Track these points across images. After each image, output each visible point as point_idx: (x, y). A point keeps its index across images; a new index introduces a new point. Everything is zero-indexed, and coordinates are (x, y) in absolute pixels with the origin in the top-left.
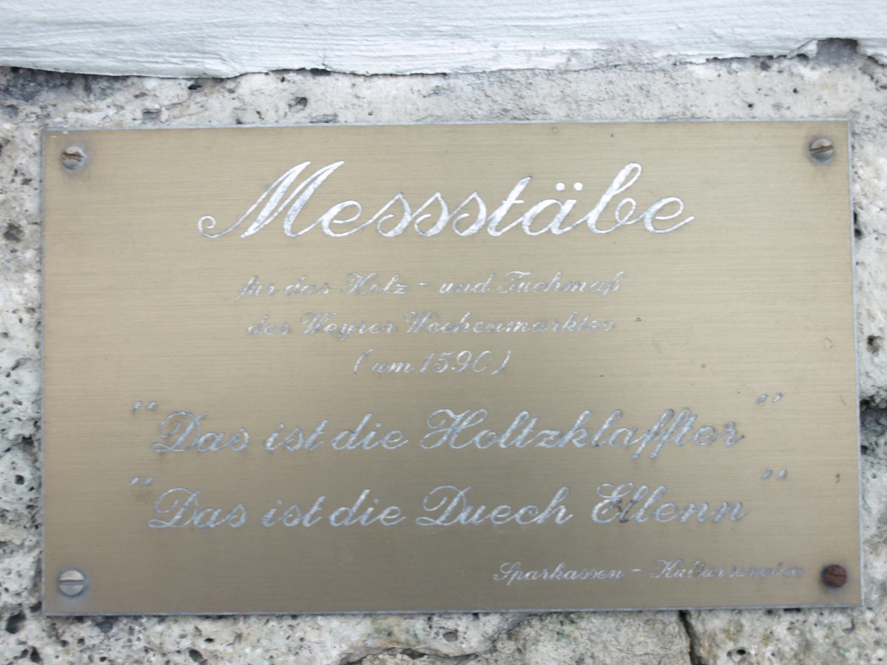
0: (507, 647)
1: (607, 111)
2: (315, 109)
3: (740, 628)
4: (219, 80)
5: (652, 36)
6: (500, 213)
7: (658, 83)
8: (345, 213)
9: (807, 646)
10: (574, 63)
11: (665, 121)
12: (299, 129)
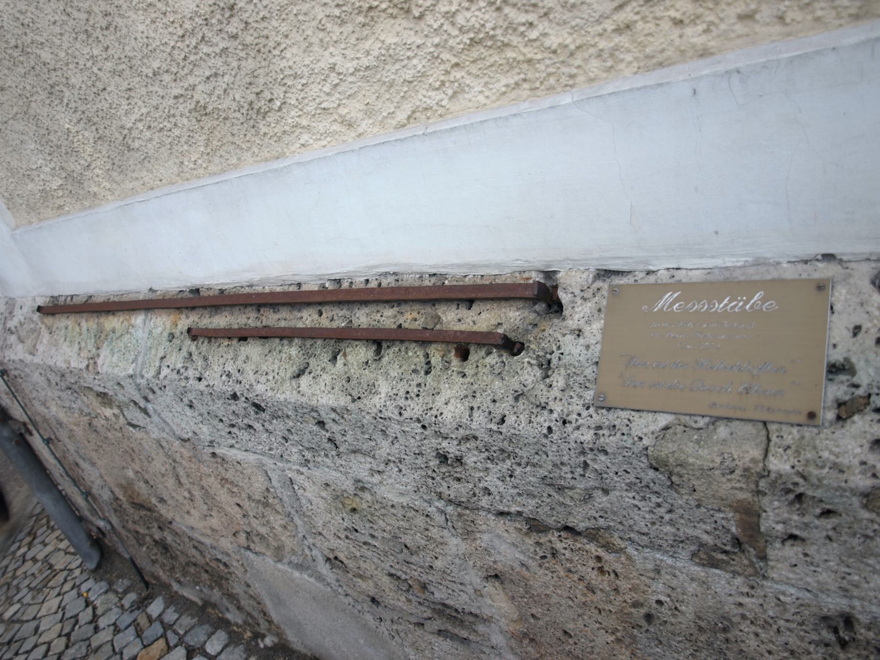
0: (711, 427)
1: (757, 278)
2: (676, 278)
3: (781, 429)
4: (654, 272)
5: (768, 255)
6: (721, 306)
7: (772, 268)
8: (680, 305)
9: (803, 438)
10: (747, 264)
11: (773, 280)
12: (671, 284)
